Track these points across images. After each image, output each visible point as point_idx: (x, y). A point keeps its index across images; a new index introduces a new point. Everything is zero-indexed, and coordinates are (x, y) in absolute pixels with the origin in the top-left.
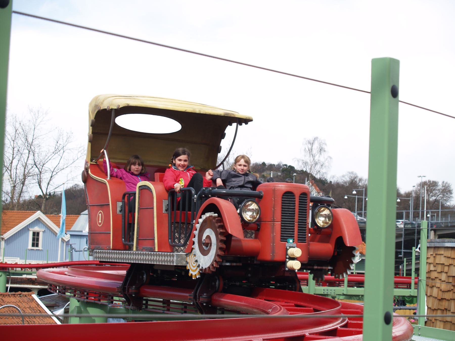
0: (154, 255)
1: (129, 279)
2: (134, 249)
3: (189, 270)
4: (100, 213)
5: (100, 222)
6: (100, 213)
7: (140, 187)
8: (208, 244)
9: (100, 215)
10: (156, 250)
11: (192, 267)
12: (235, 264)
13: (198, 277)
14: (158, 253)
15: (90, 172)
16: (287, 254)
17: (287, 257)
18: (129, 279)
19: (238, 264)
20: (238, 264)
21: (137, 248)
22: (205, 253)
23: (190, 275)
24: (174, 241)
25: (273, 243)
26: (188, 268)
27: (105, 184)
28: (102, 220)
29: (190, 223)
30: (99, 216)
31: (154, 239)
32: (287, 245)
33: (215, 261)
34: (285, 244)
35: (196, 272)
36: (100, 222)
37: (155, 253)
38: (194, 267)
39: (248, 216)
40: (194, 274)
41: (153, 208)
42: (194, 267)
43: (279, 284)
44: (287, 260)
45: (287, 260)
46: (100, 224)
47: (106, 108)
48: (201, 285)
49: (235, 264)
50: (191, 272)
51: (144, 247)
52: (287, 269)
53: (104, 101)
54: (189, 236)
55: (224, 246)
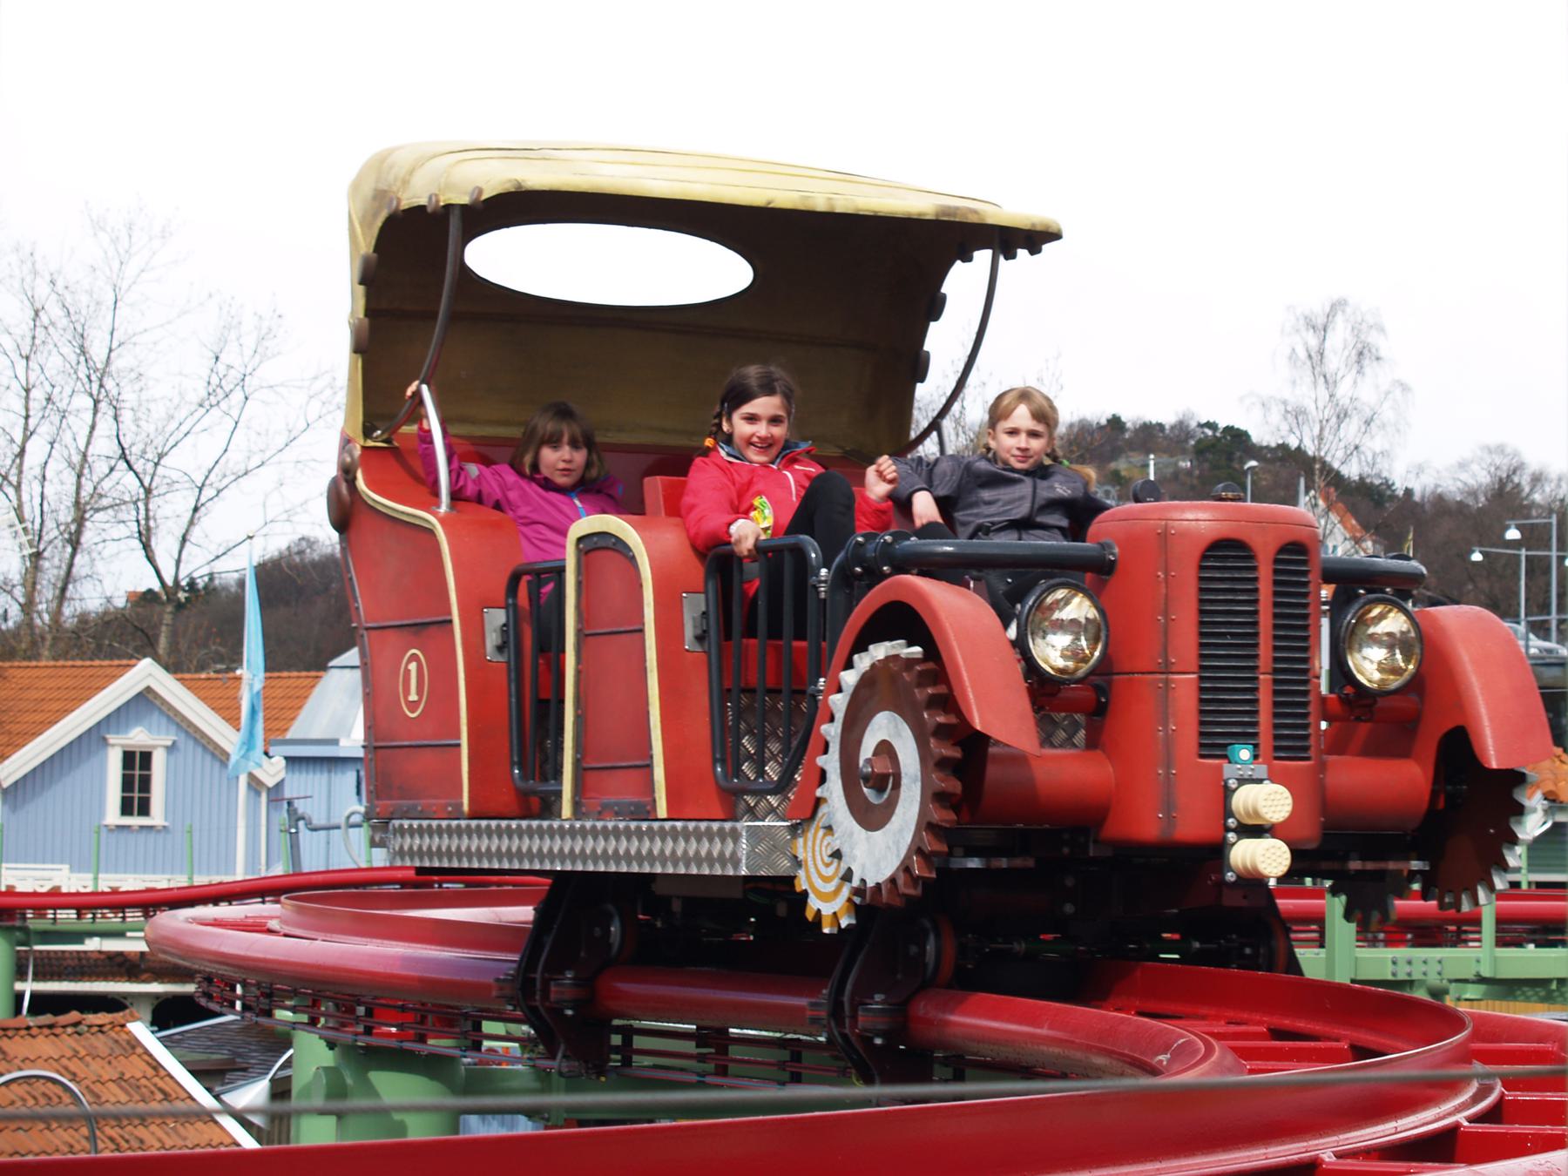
0: (651, 834)
1: (548, 941)
2: (567, 810)
3: (805, 894)
4: (414, 658)
5: (413, 697)
6: (414, 658)
7: (580, 540)
8: (887, 780)
9: (413, 666)
10: (662, 811)
11: (818, 883)
12: (1003, 863)
13: (844, 923)
14: (668, 825)
15: (361, 483)
16: (1228, 812)
17: (1231, 822)
18: (548, 941)
19: (1018, 862)
20: (1018, 862)
21: (576, 805)
22: (871, 817)
23: (810, 916)
24: (738, 772)
25: (1168, 768)
26: (802, 884)
27: (431, 532)
28: (420, 692)
29: (803, 692)
30: (407, 672)
31: (649, 767)
32: (1230, 771)
33: (917, 849)
34: (1220, 769)
35: (838, 904)
36: (413, 697)
37: (656, 825)
38: (826, 880)
39: (1052, 651)
40: (827, 910)
41: (641, 631)
42: (826, 880)
43: (1197, 945)
44: (1231, 836)
45: (1231, 836)
46: (413, 706)
47: (423, 201)
48: (861, 958)
49: (1003, 863)
50: (814, 903)
51: (605, 800)
52: (1230, 876)
53: (411, 172)
54: (801, 746)
55: (955, 786)
